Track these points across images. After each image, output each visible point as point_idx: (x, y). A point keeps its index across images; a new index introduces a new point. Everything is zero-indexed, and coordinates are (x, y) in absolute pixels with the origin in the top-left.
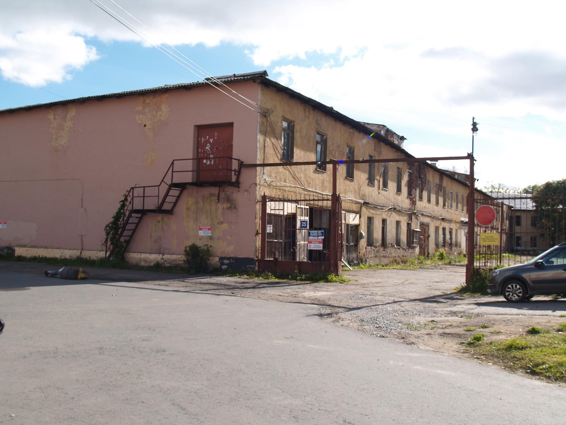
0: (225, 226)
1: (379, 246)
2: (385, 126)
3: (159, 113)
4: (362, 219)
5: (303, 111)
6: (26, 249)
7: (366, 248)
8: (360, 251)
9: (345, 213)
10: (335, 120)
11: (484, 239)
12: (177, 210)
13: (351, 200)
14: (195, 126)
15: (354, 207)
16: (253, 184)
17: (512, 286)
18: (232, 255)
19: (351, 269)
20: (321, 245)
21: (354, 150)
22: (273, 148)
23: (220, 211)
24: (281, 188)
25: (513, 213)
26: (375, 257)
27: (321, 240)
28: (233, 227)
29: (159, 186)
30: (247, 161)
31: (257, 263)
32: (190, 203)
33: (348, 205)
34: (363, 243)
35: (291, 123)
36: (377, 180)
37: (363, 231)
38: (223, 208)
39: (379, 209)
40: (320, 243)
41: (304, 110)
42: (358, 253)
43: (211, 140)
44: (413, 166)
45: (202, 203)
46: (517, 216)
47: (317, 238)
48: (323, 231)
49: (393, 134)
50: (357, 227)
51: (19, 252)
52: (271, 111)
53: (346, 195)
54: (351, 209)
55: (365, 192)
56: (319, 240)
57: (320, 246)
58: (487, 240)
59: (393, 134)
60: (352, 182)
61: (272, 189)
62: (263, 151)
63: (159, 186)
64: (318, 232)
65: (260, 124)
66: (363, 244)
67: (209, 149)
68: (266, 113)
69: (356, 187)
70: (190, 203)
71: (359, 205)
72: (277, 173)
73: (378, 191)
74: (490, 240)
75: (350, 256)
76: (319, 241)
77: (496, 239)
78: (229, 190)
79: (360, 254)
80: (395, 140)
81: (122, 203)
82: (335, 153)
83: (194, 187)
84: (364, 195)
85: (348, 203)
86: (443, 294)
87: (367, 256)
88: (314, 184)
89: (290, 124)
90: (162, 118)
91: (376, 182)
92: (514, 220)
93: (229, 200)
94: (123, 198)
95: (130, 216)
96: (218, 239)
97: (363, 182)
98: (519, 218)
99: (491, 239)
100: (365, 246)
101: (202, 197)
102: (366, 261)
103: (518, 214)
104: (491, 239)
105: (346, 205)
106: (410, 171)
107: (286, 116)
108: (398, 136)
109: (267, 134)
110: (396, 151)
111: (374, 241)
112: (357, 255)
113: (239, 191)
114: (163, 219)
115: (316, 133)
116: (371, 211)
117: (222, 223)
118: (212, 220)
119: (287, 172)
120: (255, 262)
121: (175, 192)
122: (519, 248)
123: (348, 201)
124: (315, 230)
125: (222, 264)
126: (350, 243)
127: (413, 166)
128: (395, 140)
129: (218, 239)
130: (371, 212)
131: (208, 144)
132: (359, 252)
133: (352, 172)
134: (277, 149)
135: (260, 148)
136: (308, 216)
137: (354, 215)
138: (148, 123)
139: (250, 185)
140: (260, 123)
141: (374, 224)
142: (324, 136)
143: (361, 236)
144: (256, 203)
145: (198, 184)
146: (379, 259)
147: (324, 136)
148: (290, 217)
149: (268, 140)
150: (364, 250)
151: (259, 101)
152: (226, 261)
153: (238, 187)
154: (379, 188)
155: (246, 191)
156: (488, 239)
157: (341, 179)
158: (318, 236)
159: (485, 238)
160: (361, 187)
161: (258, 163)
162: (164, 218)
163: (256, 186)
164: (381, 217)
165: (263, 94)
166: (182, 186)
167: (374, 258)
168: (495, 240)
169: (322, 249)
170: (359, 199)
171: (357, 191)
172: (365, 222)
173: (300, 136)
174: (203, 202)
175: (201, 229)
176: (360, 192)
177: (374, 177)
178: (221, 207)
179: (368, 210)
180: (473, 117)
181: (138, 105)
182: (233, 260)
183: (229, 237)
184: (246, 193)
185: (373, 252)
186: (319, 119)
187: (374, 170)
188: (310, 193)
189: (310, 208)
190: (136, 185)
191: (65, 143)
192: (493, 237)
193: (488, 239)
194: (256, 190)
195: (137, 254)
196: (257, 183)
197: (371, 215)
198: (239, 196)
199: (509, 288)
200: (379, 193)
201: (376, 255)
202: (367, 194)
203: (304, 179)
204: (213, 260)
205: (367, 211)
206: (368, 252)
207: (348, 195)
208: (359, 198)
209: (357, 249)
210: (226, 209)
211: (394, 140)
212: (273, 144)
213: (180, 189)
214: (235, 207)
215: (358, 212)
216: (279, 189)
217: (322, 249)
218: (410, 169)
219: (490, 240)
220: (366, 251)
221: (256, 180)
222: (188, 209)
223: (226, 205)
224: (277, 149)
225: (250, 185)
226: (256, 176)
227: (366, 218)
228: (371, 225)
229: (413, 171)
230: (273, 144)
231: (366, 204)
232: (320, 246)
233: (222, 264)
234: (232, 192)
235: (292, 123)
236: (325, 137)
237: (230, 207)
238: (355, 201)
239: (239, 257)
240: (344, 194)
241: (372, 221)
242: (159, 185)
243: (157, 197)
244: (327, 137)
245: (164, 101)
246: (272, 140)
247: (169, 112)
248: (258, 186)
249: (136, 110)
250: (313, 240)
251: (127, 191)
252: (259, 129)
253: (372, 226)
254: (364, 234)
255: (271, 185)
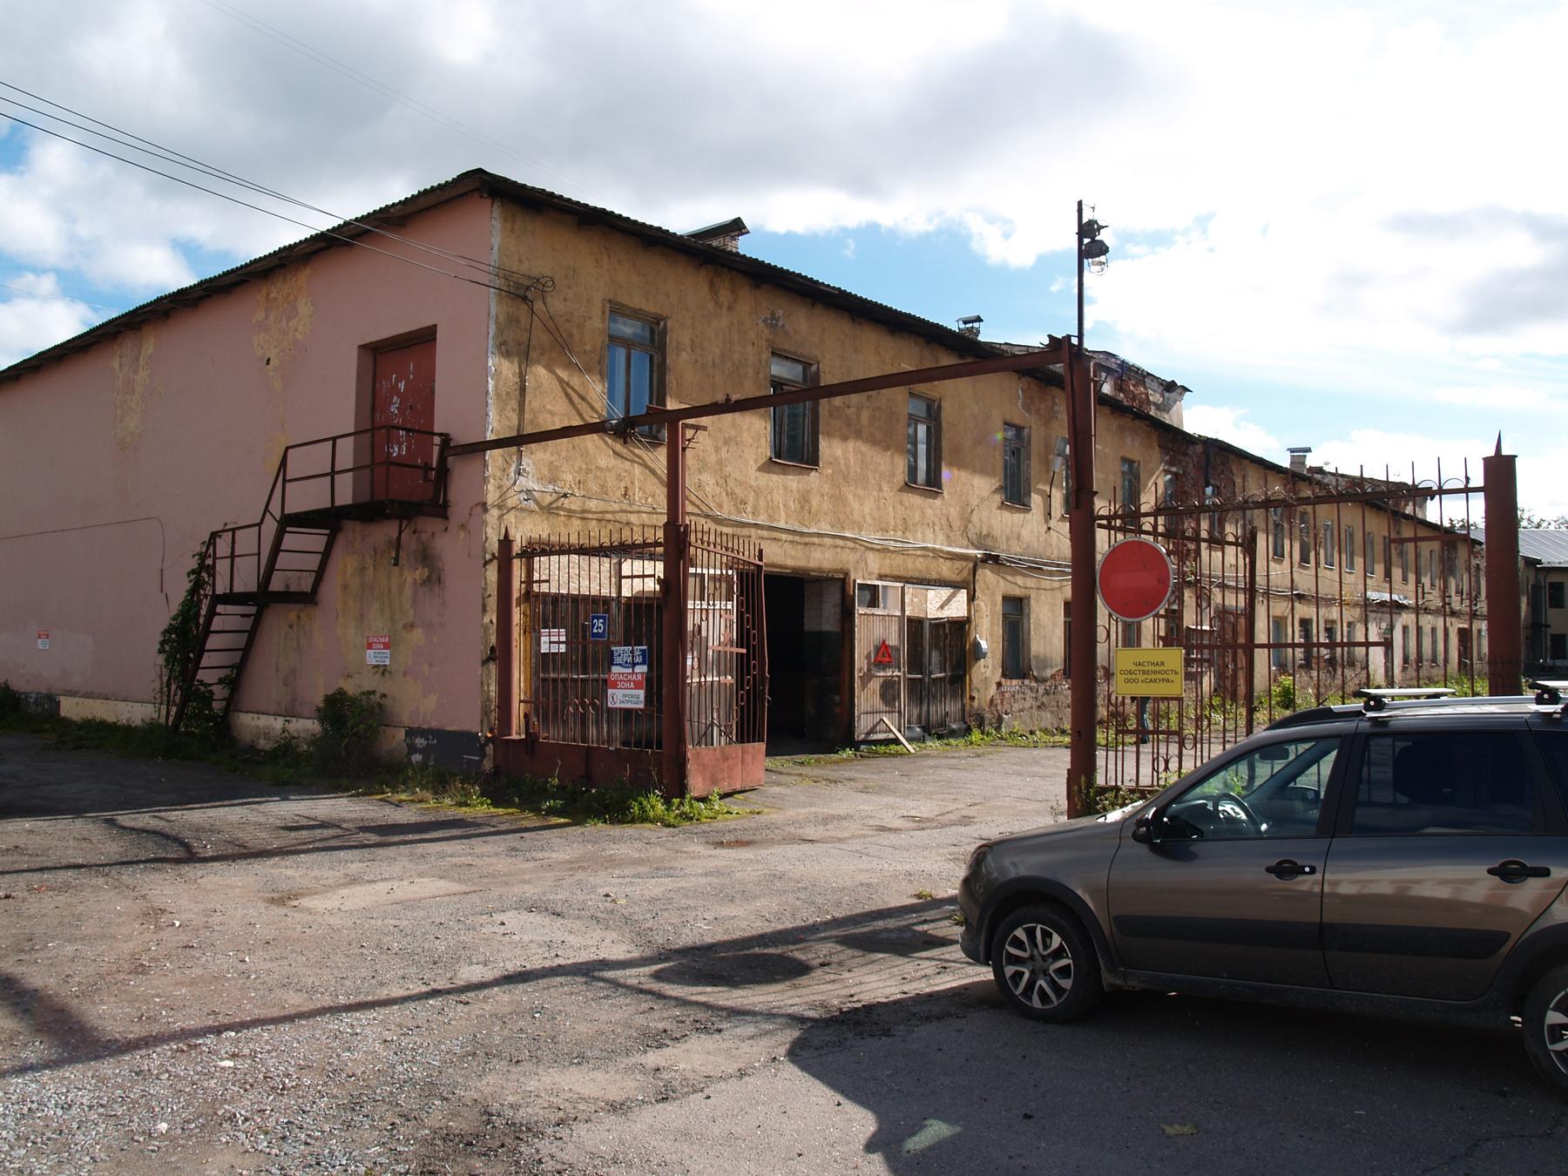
0: (418, 635)
1: (1053, 677)
2: (1114, 356)
3: (292, 323)
4: (982, 604)
5: (706, 288)
6: (77, 699)
7: (999, 684)
8: (975, 694)
9: (903, 588)
10: (853, 320)
11: (1130, 672)
12: (331, 590)
13: (934, 550)
14: (363, 347)
15: (944, 569)
16: (477, 505)
17: (1031, 933)
18: (434, 724)
19: (912, 751)
20: (641, 693)
21: (940, 407)
22: (562, 394)
23: (408, 592)
24: (609, 516)
25: (1541, 578)
26: (1039, 707)
27: (640, 677)
28: (435, 640)
29: (259, 525)
30: (462, 436)
31: (490, 749)
32: (349, 571)
33: (918, 565)
34: (986, 672)
35: (658, 324)
36: (1040, 492)
37: (988, 636)
38: (415, 580)
39: (1051, 573)
40: (637, 686)
41: (712, 285)
42: (967, 701)
43: (402, 386)
44: (1185, 454)
45: (372, 568)
46: (1551, 584)
47: (630, 670)
48: (645, 647)
49: (1142, 376)
50: (959, 627)
51: (71, 708)
52: (550, 283)
53: (908, 534)
54: (934, 576)
55: (991, 527)
56: (634, 678)
57: (638, 697)
58: (1142, 677)
59: (1144, 377)
60: (935, 498)
61: (563, 519)
62: (514, 404)
63: (259, 525)
64: (632, 652)
65: (497, 323)
66: (988, 674)
67: (396, 411)
68: (528, 288)
69: (954, 513)
70: (349, 571)
71: (965, 564)
72: (589, 471)
73: (1047, 522)
74: (1153, 677)
75: (932, 709)
76: (634, 681)
77: (1176, 673)
78: (428, 525)
79: (976, 704)
80: (1150, 392)
81: (192, 577)
82: (859, 415)
83: (358, 522)
84: (988, 535)
85: (921, 560)
86: (915, 901)
87: (1006, 707)
88: (762, 503)
89: (655, 327)
90: (299, 336)
91: (1036, 500)
92: (1546, 595)
93: (426, 557)
94: (193, 564)
95: (212, 613)
96: (405, 674)
97: (983, 500)
98: (1557, 589)
99: (1155, 672)
100: (998, 676)
101: (372, 553)
102: (1000, 720)
103: (1554, 578)
104: (1155, 672)
105: (910, 565)
106: (1174, 469)
107: (625, 300)
108: (1161, 382)
109: (533, 355)
110: (1112, 413)
111: (1033, 663)
112: (963, 705)
113: (446, 529)
114: (299, 617)
115: (766, 355)
116: (1020, 580)
117: (412, 626)
118: (392, 619)
119: (637, 469)
120: (483, 746)
121: (314, 540)
122: (1559, 663)
123: (919, 552)
124: (625, 645)
125: (413, 749)
126: (931, 673)
127: (1185, 454)
128: (1150, 392)
129: (405, 674)
130: (1019, 582)
131: (395, 398)
132: (972, 698)
133: (935, 470)
134: (582, 398)
135: (498, 395)
136: (729, 598)
137: (945, 592)
138: (272, 353)
139: (471, 509)
140: (501, 318)
141: (1032, 616)
142: (811, 364)
143: (977, 653)
144: (486, 563)
145: (367, 511)
146: (1052, 712)
147: (811, 364)
148: (650, 602)
149: (540, 372)
150: (993, 690)
151: (496, 250)
152: (420, 742)
153: (446, 517)
154: (1050, 514)
155: (463, 527)
156: (1144, 672)
157: (885, 488)
158: (634, 665)
159: (1134, 668)
160: (972, 511)
161: (490, 436)
162: (302, 615)
163: (486, 510)
164: (1059, 595)
165: (512, 230)
166: (328, 520)
167: (1034, 711)
168: (1171, 677)
169: (642, 706)
170: (967, 548)
171: (957, 524)
172: (993, 612)
173: (696, 361)
174: (374, 566)
175: (370, 647)
176: (970, 526)
177: (1029, 485)
178: (410, 580)
179: (1004, 578)
180: (1080, 203)
181: (249, 309)
182: (433, 739)
183: (426, 668)
184: (462, 534)
185: (1029, 694)
186: (780, 313)
187: (1029, 465)
188: (745, 531)
189: (740, 575)
190: (226, 524)
191: (136, 427)
192: (1163, 663)
193: (1144, 672)
194: (485, 523)
195: (251, 715)
196: (489, 502)
197: (1017, 592)
198: (449, 546)
199: (1018, 944)
200: (1049, 529)
201: (1043, 703)
202: (997, 532)
203: (718, 490)
204: (394, 737)
205: (1002, 581)
206: (1007, 695)
207: (920, 535)
208: (965, 542)
209: (963, 690)
210: (421, 585)
211: (1147, 395)
212: (561, 380)
213: (327, 532)
214: (439, 579)
215: (968, 584)
216: (599, 520)
217: (642, 706)
218: (1171, 463)
219: (1153, 677)
220: (1003, 694)
221: (483, 493)
222: (345, 587)
223: (421, 573)
224: (582, 398)
225: (471, 509)
226: (485, 480)
227: (1000, 599)
228: (1022, 619)
229: (1185, 468)
230: (561, 380)
231: (992, 560)
232: (638, 697)
233: (413, 749)
234: (433, 534)
235: (662, 323)
236: (814, 368)
237: (429, 579)
238: (949, 553)
239: (449, 729)
240: (899, 533)
241: (1026, 608)
242: (258, 521)
243: (256, 557)
244: (818, 368)
245: (303, 285)
246: (560, 372)
247: (312, 316)
248: (495, 512)
249: (254, 321)
250: (621, 678)
251: (203, 543)
252: (495, 338)
253: (1025, 621)
254: (984, 645)
255: (558, 508)
